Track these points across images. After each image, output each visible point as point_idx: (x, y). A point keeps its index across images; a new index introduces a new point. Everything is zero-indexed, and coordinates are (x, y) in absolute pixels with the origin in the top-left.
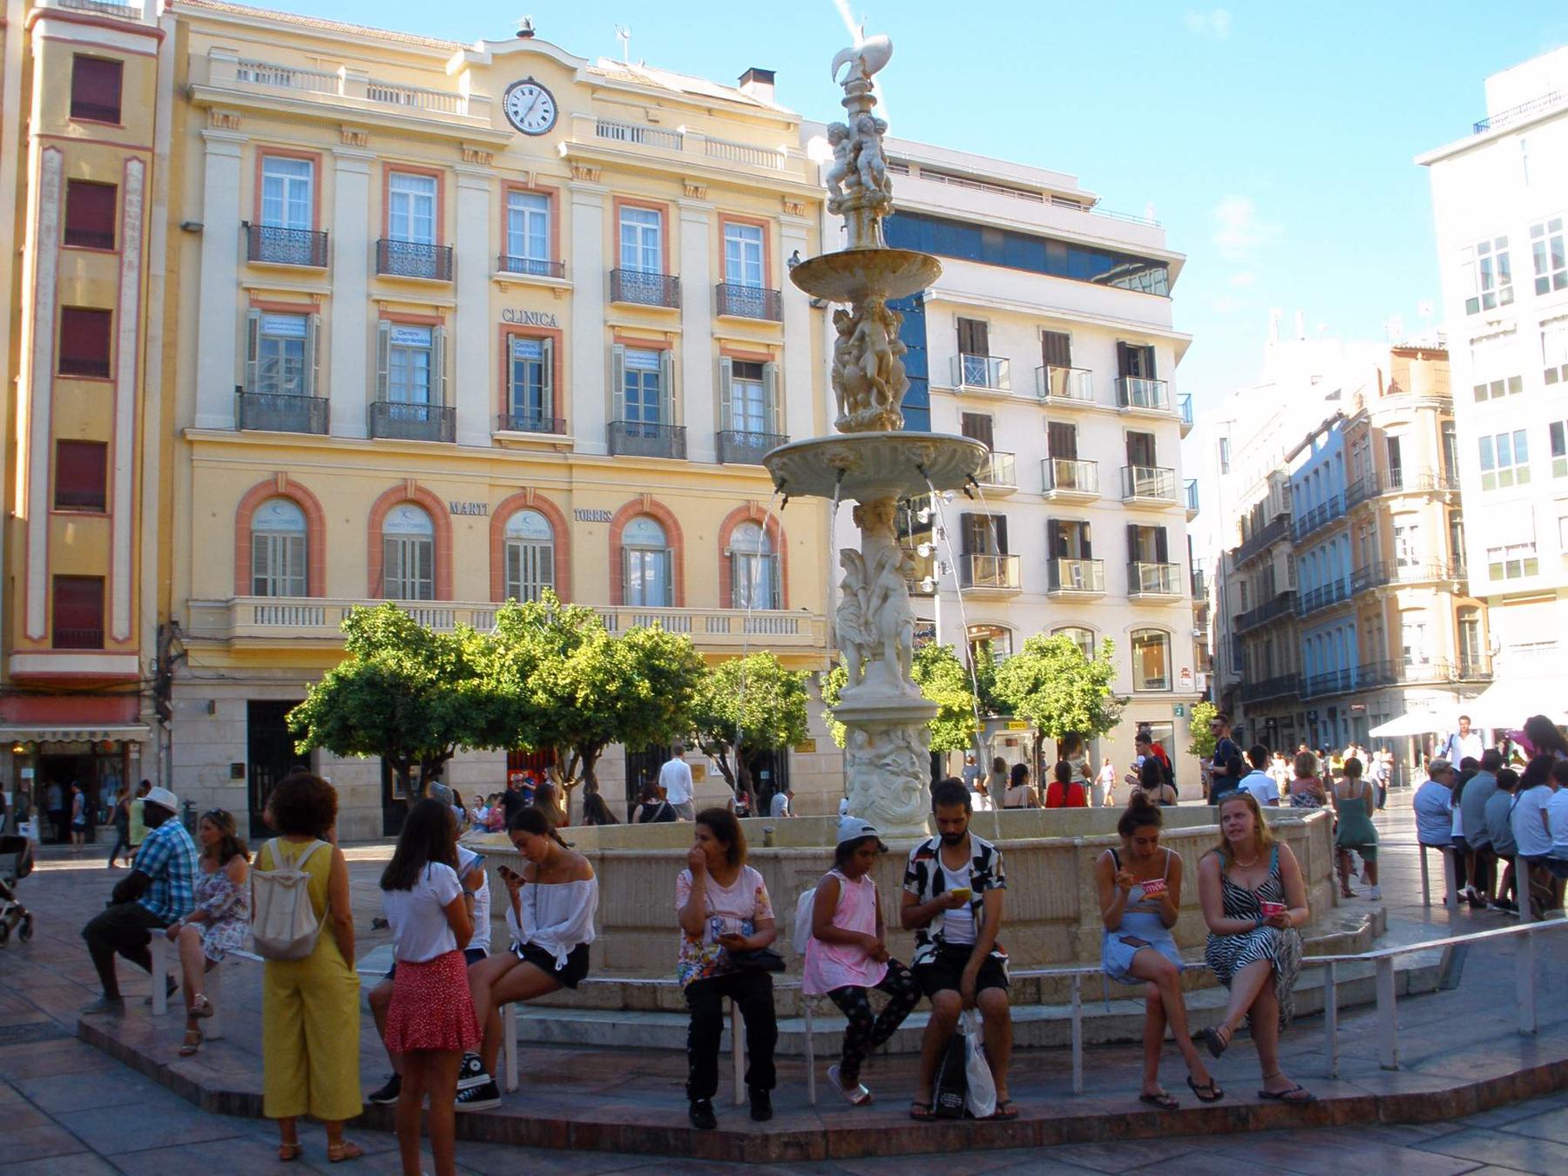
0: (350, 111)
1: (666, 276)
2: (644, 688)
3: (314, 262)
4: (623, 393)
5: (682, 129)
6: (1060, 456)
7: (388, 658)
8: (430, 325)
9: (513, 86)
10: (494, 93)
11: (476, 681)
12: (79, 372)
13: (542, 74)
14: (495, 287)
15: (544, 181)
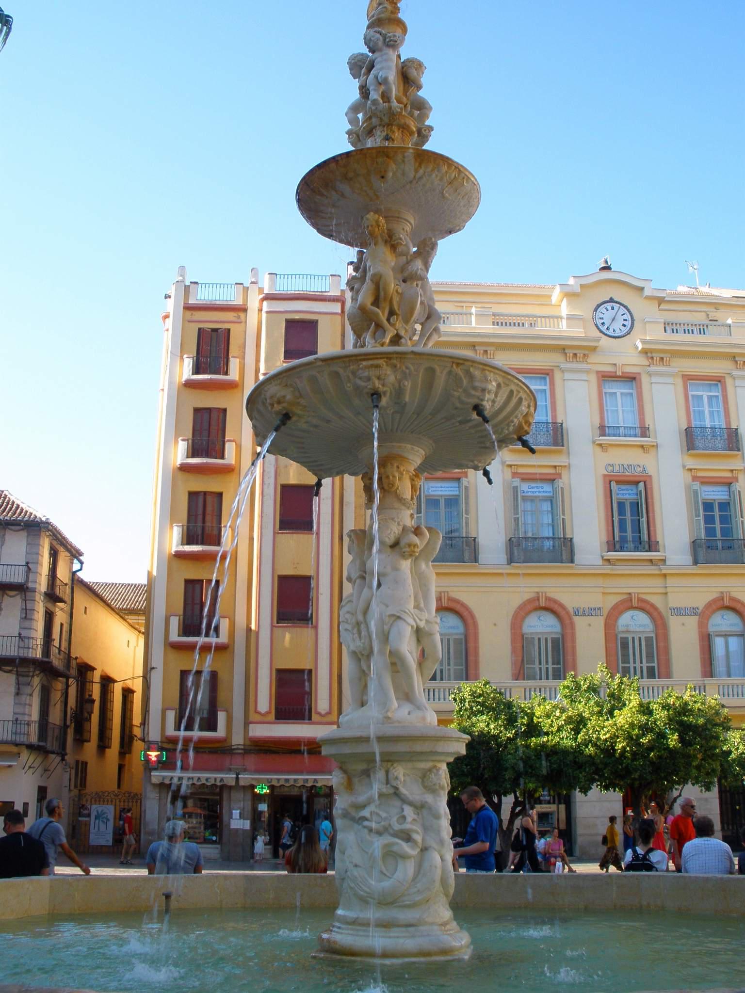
0: (479, 335)
1: (729, 428)
2: (673, 740)
3: (555, 443)
4: (701, 518)
5: (729, 321)
6: (363, 532)
7: (482, 723)
8: (728, 484)
9: (599, 306)
10: (585, 310)
11: (545, 739)
12: (289, 529)
13: (619, 294)
14: (598, 449)
15: (628, 370)
